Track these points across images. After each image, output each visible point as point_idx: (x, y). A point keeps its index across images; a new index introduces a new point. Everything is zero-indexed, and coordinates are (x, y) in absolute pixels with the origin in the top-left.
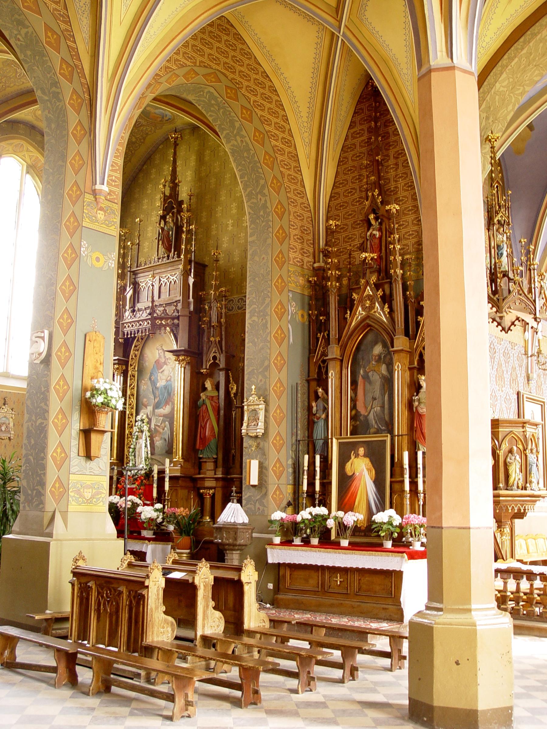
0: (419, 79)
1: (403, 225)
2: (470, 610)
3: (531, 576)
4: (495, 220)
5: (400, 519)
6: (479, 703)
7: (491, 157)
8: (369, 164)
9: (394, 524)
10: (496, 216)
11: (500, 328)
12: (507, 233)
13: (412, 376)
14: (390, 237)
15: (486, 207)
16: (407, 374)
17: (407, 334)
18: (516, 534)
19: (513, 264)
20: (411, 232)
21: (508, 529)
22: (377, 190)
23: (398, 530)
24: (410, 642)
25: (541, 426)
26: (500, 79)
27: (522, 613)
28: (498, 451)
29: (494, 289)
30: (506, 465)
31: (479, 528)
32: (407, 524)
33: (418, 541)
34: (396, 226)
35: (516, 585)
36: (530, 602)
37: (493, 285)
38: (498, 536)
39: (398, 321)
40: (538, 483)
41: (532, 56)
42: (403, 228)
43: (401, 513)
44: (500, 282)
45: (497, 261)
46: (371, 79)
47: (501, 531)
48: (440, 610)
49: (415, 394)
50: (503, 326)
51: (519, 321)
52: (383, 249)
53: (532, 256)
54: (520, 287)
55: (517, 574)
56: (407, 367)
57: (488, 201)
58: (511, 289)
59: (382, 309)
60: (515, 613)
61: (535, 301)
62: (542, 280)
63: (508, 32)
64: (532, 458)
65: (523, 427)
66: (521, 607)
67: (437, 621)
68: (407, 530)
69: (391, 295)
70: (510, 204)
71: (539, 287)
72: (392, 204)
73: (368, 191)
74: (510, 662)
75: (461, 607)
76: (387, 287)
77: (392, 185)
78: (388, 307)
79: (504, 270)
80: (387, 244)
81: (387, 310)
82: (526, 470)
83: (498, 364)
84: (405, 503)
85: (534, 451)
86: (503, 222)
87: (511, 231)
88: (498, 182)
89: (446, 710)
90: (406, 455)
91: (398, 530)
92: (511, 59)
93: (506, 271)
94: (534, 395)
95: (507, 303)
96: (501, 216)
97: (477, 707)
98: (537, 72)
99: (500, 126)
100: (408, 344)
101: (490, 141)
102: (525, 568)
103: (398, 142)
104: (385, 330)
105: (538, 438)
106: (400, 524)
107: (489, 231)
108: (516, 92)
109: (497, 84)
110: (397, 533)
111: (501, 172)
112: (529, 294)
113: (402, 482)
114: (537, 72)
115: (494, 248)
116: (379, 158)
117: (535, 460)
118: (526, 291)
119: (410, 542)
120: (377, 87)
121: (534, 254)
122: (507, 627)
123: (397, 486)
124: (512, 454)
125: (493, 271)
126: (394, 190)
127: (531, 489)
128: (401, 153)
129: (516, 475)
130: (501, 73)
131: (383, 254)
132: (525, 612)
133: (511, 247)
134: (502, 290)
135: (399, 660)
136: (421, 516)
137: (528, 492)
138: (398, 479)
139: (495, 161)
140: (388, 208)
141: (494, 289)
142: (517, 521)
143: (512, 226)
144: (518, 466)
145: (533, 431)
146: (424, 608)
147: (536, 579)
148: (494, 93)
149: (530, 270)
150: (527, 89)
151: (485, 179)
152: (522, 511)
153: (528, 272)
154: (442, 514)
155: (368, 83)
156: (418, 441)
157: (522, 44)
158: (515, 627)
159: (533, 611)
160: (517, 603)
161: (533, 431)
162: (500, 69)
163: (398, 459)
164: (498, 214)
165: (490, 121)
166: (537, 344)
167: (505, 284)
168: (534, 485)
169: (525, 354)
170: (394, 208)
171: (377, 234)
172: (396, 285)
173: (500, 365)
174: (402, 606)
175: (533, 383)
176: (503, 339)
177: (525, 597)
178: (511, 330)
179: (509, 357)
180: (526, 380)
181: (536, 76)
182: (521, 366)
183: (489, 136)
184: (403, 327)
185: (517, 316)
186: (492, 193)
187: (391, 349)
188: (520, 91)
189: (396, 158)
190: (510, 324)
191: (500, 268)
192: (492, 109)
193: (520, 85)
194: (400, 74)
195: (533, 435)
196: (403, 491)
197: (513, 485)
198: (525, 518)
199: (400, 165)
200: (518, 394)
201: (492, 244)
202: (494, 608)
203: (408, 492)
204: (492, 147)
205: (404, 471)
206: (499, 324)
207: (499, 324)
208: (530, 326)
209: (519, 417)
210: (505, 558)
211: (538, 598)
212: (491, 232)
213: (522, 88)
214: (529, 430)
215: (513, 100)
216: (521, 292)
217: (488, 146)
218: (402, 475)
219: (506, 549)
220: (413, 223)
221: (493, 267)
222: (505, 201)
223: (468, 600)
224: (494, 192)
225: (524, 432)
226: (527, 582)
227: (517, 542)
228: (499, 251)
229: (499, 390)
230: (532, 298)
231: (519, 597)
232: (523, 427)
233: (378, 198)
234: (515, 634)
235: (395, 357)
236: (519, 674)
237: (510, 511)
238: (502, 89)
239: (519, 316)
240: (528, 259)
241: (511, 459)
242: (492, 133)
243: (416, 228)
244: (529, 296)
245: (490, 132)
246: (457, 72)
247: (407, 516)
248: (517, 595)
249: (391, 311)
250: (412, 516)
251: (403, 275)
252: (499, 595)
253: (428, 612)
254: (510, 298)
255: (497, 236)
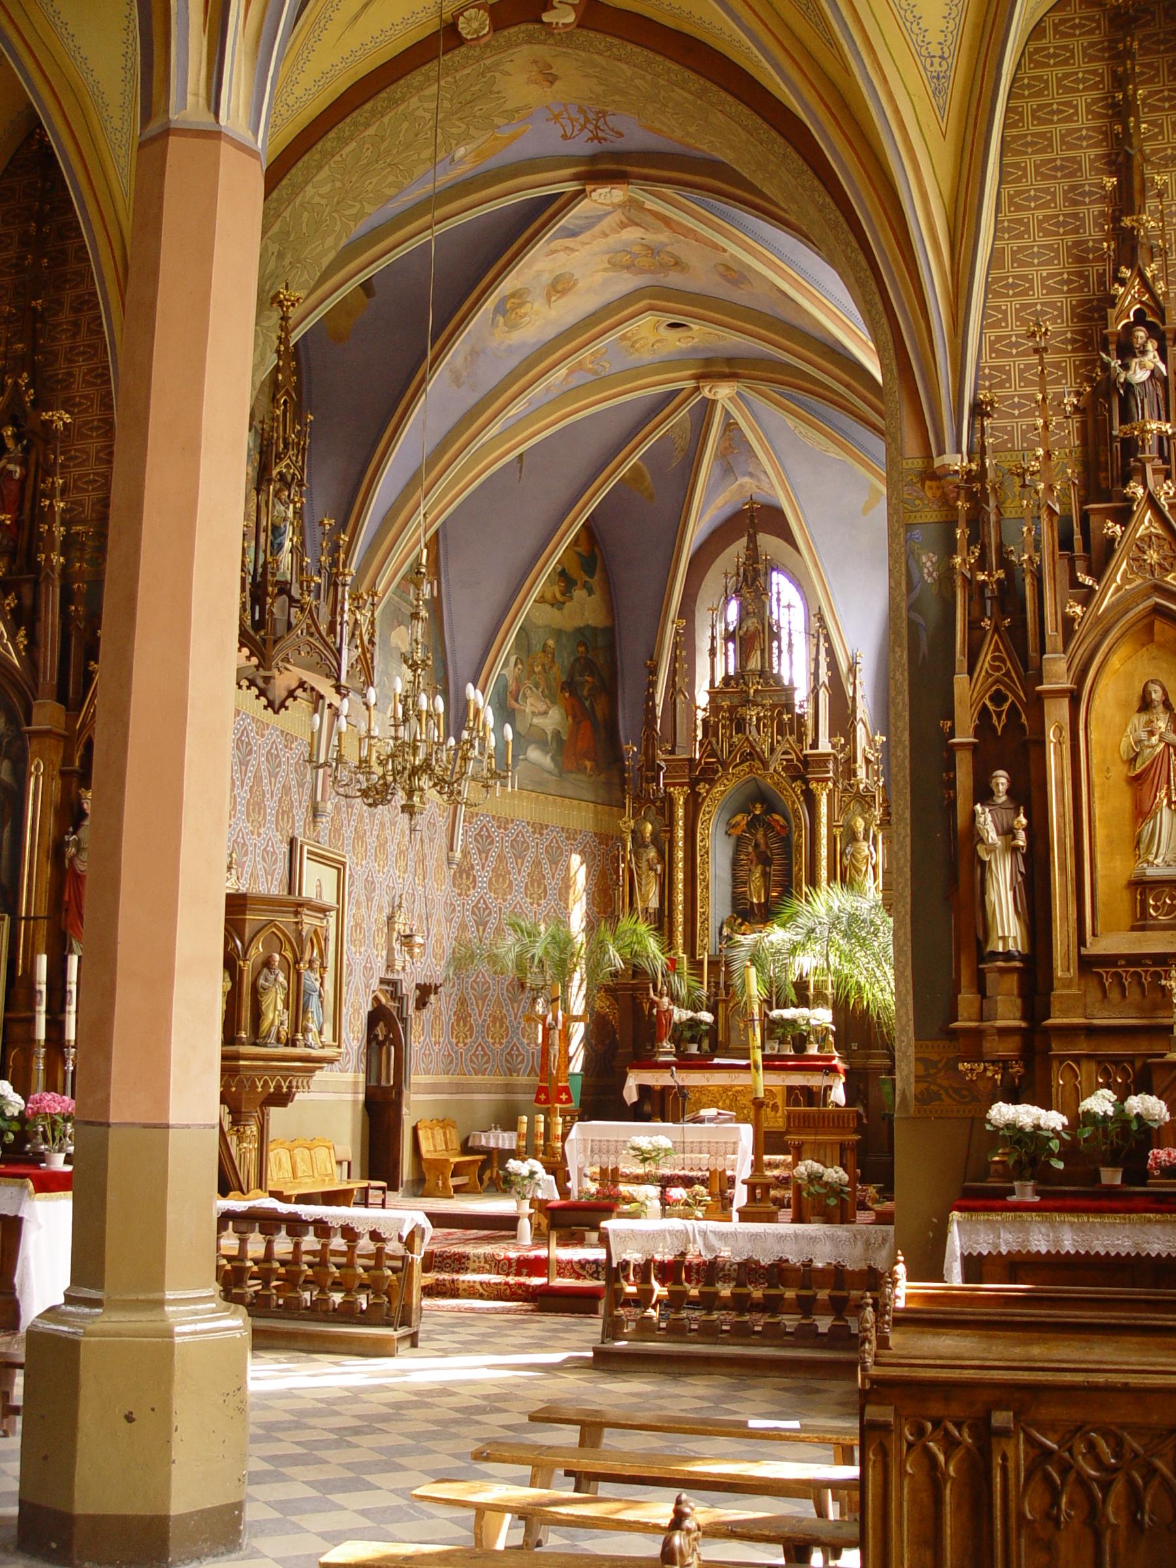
0: (141, 146)
1: (76, 458)
2: (161, 1303)
3: (296, 1225)
4: (274, 473)
5: (22, 1102)
6: (172, 1500)
7: (279, 338)
8: (14, 314)
9: (8, 1114)
10: (276, 464)
11: (263, 701)
12: (295, 503)
13: (66, 790)
14: (44, 482)
15: (259, 441)
16: (56, 785)
17: (62, 697)
18: (270, 1139)
19: (302, 569)
20: (91, 477)
21: (254, 1129)
22: (25, 375)
23: (16, 1126)
24: (26, 1377)
25: (333, 913)
26: (315, 180)
27: (274, 1304)
28: (241, 963)
29: (257, 617)
30: (256, 992)
31: (188, 1126)
32: (36, 1113)
33: (60, 1151)
34: (61, 459)
35: (264, 1245)
36: (292, 1280)
37: (257, 608)
38: (232, 1140)
39: (45, 667)
40: (321, 1033)
41: (385, 144)
42: (75, 466)
43: (22, 1089)
44: (272, 604)
45: (270, 559)
46: (40, 125)
47: (238, 1131)
48: (96, 1303)
49: (71, 829)
50: (271, 698)
51: (305, 690)
52: (27, 505)
53: (342, 556)
54: (313, 620)
55: (268, 1222)
56: (57, 768)
57: (263, 429)
58: (294, 621)
59: (12, 638)
60: (257, 1307)
61: (340, 650)
62: (358, 608)
63: (342, 84)
64: (311, 979)
65: (296, 913)
66: (274, 1291)
67: (90, 1327)
68: (36, 1126)
69: (35, 609)
70: (308, 441)
71: (351, 624)
72: (57, 410)
73: (5, 373)
74: (242, 1410)
75: (142, 1297)
76: (26, 590)
77: (61, 369)
78: (26, 636)
79: (282, 579)
80: (38, 495)
81: (22, 639)
82: (298, 1004)
83: (255, 776)
84: (35, 1067)
85: (317, 964)
86: (289, 478)
87: (304, 500)
88: (288, 393)
89: (98, 1521)
90: (42, 961)
91: (16, 1126)
92: (345, 142)
93: (286, 583)
94: (325, 848)
95: (280, 651)
96: (288, 466)
97: (168, 1509)
98: (391, 179)
99: (306, 276)
100: (63, 719)
101: (281, 303)
102: (283, 1208)
103: (85, 276)
104: (15, 684)
105: (326, 939)
106: (20, 1112)
107: (258, 494)
108: (346, 213)
109: (309, 188)
110: (14, 1133)
111: (297, 372)
112: (328, 634)
113: (31, 1021)
114: (391, 179)
115: (266, 530)
116: (38, 304)
117: (318, 984)
118: (323, 628)
119: (42, 1154)
120: (51, 147)
121: (347, 554)
122: (238, 1336)
123: (18, 1030)
124: (269, 969)
125: (259, 579)
126: (65, 380)
127: (306, 1046)
128: (88, 302)
129: (276, 1014)
130: (320, 168)
131: (26, 516)
132: (281, 1302)
133: (302, 533)
134: (274, 621)
135: (5, 1415)
136: (67, 1098)
137: (299, 1051)
138: (22, 1015)
139: (287, 348)
140: (45, 416)
141: (257, 617)
142: (274, 1112)
143: (310, 490)
144: (281, 996)
145: (317, 922)
146: (61, 1300)
147: (306, 1234)
148: (301, 205)
149: (336, 585)
150: (369, 209)
151: (263, 383)
152: (285, 1090)
153: (332, 588)
154: (109, 1095)
155: (30, 136)
156: (70, 932)
157: (367, 115)
158: (256, 1332)
159: (298, 1299)
160: (266, 1285)
161: (317, 922)
162: (317, 156)
163: (24, 970)
164: (281, 459)
165: (287, 261)
166: (336, 743)
167: (282, 609)
168: (311, 1038)
169: (310, 761)
170: (61, 418)
171: (17, 471)
172: (47, 588)
173: (257, 778)
174: (18, 1294)
175: (324, 822)
176: (268, 725)
177: (282, 1270)
178: (287, 708)
179: (279, 765)
180: (310, 814)
181: (389, 186)
182: (301, 785)
183: (279, 293)
184: (55, 682)
185: (300, 679)
186: (273, 413)
187: (26, 728)
188: (354, 211)
189: (76, 310)
190: (285, 694)
191: (274, 575)
192: (291, 239)
193: (354, 199)
194: (106, 129)
195: (316, 932)
196: (31, 1040)
197: (268, 1035)
198: (290, 1104)
199: (84, 329)
200: (292, 842)
201: (264, 523)
202: (212, 1297)
203: (42, 1043)
204: (284, 318)
205: (35, 997)
206: (262, 693)
207: (262, 693)
208: (327, 702)
209: (290, 893)
210: (245, 1190)
211: (310, 1272)
212: (263, 497)
213: (358, 205)
214: (309, 921)
215: (337, 228)
216: (313, 629)
217: (275, 315)
218: (31, 1005)
219: (247, 1170)
220: (97, 458)
221: (260, 570)
222: (299, 434)
223: (156, 1280)
224: (278, 412)
225: (297, 923)
226: (288, 1240)
227: (271, 1155)
228: (275, 538)
229: (252, 833)
230: (335, 643)
231: (272, 1271)
232: (296, 913)
233: (26, 391)
234: (256, 1348)
235: (33, 747)
236: (261, 1432)
237: (260, 1089)
238: (317, 200)
239: (305, 679)
240: (334, 563)
241: (266, 980)
242: (287, 288)
243: (102, 468)
244: (330, 640)
245: (284, 285)
246: (225, 148)
247: (37, 1096)
248: (266, 1265)
249: (33, 644)
250: (49, 1097)
251: (65, 567)
252: (228, 1267)
253: (70, 1309)
254: (290, 639)
255: (274, 505)
